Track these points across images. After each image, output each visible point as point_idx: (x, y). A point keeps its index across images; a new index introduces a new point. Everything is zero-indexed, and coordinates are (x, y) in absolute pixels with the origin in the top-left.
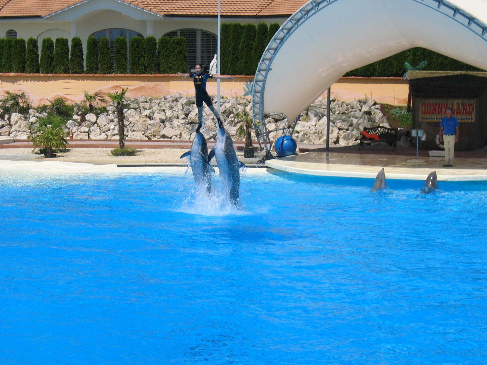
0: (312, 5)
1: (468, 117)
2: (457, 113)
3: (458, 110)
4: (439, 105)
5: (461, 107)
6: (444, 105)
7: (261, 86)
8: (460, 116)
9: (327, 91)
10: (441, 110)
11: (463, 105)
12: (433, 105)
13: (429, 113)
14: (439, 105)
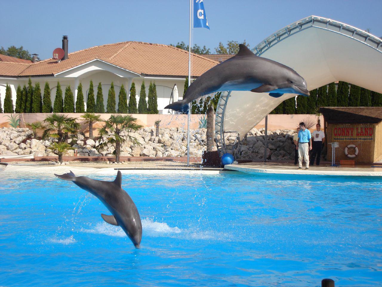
0: (266, 43)
1: (369, 138)
2: (361, 135)
3: (361, 132)
4: (347, 129)
5: (364, 131)
6: (351, 129)
7: (225, 100)
8: (363, 137)
9: (265, 118)
10: (349, 133)
11: (365, 129)
12: (343, 129)
13: (339, 135)
14: (347, 129)
